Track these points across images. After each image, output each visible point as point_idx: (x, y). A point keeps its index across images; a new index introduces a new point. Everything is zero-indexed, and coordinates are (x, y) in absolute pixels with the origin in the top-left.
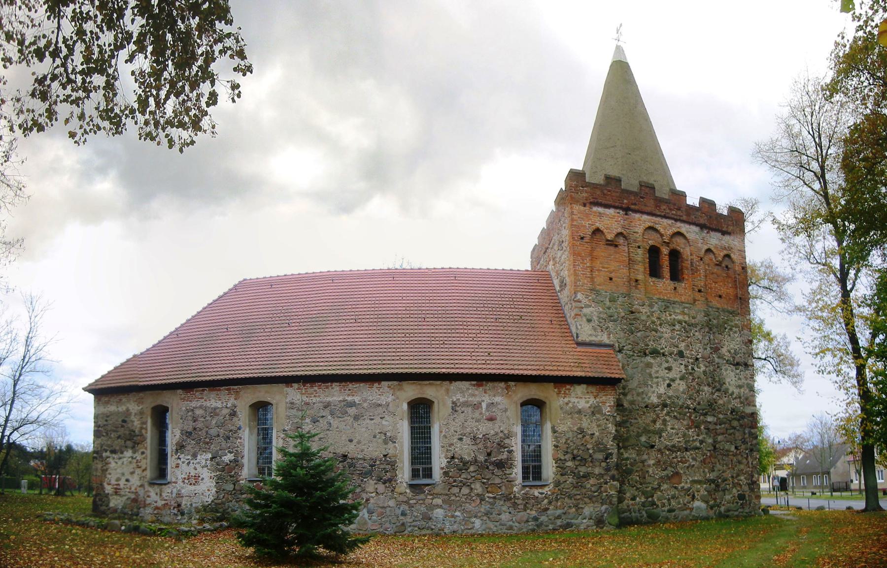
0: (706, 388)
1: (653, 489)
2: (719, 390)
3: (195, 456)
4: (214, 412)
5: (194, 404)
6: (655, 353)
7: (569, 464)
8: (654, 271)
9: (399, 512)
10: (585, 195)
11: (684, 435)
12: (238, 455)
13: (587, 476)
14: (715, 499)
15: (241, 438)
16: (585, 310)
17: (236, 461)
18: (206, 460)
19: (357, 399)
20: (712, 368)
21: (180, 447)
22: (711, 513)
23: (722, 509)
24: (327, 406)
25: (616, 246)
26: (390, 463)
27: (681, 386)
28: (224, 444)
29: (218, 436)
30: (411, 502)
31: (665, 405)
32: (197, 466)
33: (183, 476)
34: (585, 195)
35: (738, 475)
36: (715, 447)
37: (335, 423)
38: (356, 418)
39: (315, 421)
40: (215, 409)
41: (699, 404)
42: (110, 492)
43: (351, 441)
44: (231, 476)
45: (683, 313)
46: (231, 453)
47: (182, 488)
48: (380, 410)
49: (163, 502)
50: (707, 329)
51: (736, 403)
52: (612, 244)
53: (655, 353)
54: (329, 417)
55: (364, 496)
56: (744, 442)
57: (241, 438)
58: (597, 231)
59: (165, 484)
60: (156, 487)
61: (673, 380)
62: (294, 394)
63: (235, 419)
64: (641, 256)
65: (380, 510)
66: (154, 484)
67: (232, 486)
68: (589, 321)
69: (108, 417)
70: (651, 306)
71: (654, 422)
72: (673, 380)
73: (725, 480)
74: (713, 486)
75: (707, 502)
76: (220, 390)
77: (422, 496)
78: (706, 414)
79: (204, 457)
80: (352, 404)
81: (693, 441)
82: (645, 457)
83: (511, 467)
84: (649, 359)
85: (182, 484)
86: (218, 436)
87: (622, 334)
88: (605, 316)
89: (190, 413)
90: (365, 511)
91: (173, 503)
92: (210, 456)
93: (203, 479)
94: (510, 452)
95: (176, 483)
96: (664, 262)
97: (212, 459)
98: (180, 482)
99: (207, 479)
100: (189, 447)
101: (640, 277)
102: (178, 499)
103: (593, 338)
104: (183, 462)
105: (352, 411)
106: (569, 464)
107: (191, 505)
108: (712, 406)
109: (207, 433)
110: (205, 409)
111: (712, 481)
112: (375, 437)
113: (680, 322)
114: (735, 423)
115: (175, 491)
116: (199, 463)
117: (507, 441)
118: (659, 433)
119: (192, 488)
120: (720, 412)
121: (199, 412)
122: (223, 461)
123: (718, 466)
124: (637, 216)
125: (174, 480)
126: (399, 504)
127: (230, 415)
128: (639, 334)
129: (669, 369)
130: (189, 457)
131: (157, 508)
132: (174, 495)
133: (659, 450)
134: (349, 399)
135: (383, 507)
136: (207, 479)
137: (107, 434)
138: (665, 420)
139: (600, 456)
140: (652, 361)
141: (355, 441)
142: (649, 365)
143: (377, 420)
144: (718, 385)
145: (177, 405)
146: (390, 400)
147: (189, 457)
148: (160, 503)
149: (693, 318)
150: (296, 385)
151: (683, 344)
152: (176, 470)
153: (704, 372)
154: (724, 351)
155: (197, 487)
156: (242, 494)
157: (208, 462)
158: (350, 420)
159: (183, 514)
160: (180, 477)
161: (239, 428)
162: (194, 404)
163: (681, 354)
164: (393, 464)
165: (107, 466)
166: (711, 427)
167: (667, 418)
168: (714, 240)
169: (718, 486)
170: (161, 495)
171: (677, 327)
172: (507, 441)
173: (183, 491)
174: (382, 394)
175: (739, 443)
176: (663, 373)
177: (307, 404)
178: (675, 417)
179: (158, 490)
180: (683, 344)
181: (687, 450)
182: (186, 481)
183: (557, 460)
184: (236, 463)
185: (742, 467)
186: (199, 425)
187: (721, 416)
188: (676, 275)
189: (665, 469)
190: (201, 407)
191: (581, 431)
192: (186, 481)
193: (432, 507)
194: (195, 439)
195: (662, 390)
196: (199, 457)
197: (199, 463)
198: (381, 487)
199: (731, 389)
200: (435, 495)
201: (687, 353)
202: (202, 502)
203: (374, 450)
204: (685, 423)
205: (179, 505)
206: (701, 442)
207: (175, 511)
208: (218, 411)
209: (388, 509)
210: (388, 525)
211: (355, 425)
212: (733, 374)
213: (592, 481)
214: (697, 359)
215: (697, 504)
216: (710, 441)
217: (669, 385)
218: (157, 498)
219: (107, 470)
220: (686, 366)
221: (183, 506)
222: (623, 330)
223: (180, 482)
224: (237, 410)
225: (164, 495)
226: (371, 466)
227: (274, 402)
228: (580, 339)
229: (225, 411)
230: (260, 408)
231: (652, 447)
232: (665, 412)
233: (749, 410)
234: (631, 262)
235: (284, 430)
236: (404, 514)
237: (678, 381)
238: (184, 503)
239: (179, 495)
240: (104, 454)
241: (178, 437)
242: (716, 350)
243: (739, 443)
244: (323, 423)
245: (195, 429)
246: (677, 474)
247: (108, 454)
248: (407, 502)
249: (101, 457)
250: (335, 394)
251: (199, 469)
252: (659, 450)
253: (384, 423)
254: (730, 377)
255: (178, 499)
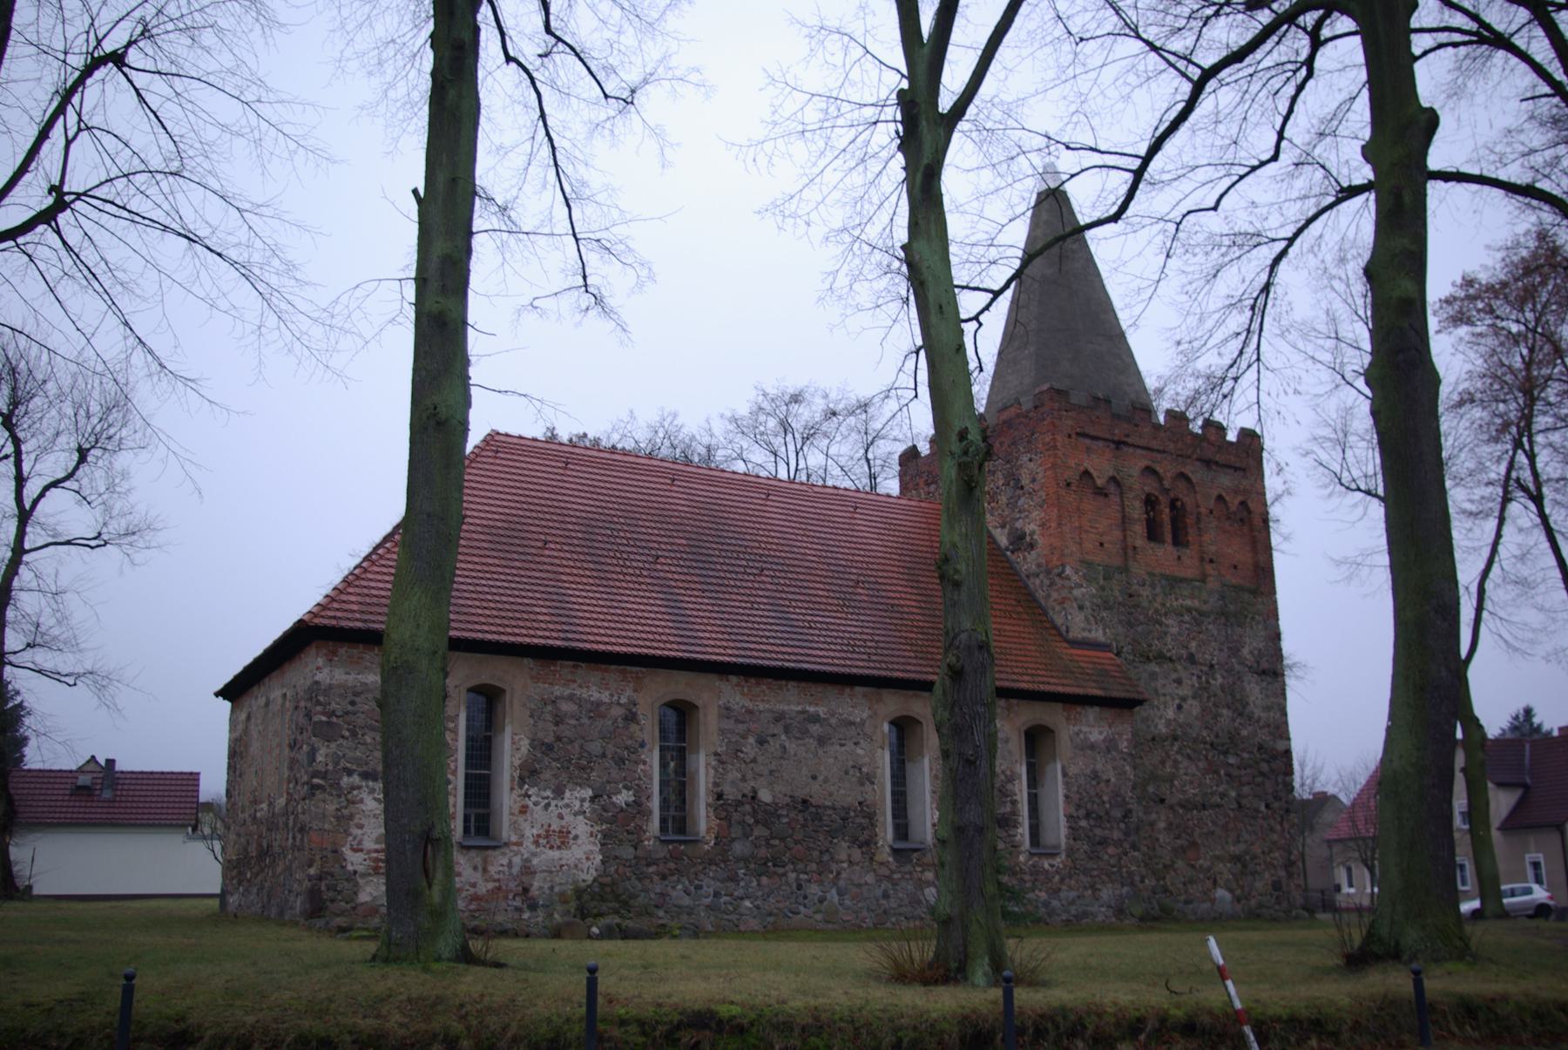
0: (1225, 711)
1: (1165, 866)
2: (1241, 714)
3: (559, 792)
4: (596, 710)
5: (558, 690)
6: (1161, 657)
7: (1083, 823)
8: (1153, 534)
9: (879, 892)
10: (1070, 422)
11: (1200, 785)
12: (641, 793)
13: (1104, 842)
14: (1242, 888)
15: (645, 763)
16: (1077, 592)
17: (637, 803)
18: (583, 800)
19: (821, 711)
20: (1231, 680)
21: (528, 774)
22: (1238, 907)
23: (1253, 902)
24: (779, 717)
25: (1106, 495)
26: (868, 814)
27: (1193, 707)
28: (615, 774)
29: (604, 755)
30: (896, 876)
31: (1175, 739)
32: (564, 811)
33: (535, 832)
34: (1070, 422)
35: (1271, 851)
36: (1239, 803)
37: (792, 747)
38: (822, 741)
39: (761, 742)
40: (599, 704)
41: (1217, 736)
42: (361, 869)
43: (814, 778)
44: (629, 832)
45: (1192, 597)
46: (628, 788)
47: (534, 854)
48: (852, 731)
49: (490, 885)
50: (1223, 620)
51: (1263, 736)
52: (1101, 492)
53: (1161, 657)
54: (783, 737)
55: (834, 867)
56: (1277, 798)
57: (645, 763)
58: (1086, 473)
59: (494, 848)
60: (473, 853)
61: (1184, 699)
62: (732, 694)
63: (634, 727)
64: (1137, 510)
65: (855, 890)
66: (469, 848)
67: (631, 850)
68: (1081, 608)
69: (356, 694)
70: (1153, 586)
71: (1163, 763)
72: (1184, 699)
73: (1254, 857)
74: (1239, 866)
75: (1231, 891)
76: (606, 671)
77: (908, 868)
78: (1226, 753)
79: (578, 796)
80: (815, 719)
81: (1213, 794)
82: (1154, 816)
83: (1016, 825)
84: (1154, 667)
85: (533, 848)
86: (604, 755)
87: (1120, 629)
88: (1099, 601)
89: (549, 708)
90: (834, 891)
91: (512, 885)
92: (590, 792)
93: (576, 837)
94: (1014, 803)
95: (519, 844)
96: (1168, 520)
97: (592, 799)
98: (528, 844)
99: (583, 838)
100: (547, 775)
101: (1139, 542)
102: (525, 879)
103: (1086, 634)
104: (536, 804)
105: (815, 729)
106: (1083, 823)
107: (551, 888)
108: (1233, 737)
109: (581, 747)
110: (580, 702)
111: (1237, 859)
112: (847, 773)
113: (1189, 610)
114: (1265, 767)
115: (517, 860)
116: (567, 806)
117: (1009, 786)
118: (1171, 779)
119: (556, 854)
120: (1243, 750)
121: (566, 707)
122: (614, 804)
123: (1246, 836)
124: (1131, 450)
125: (514, 838)
126: (880, 879)
127: (626, 719)
128: (1139, 629)
129: (1179, 682)
130: (548, 793)
131: (475, 898)
132: (515, 870)
133: (1171, 808)
134: (812, 709)
135: (859, 886)
136: (583, 838)
137: (354, 734)
138: (1175, 761)
139: (1117, 813)
140: (1157, 669)
141: (821, 778)
142: (1153, 676)
143: (850, 746)
144: (1240, 707)
145: (522, 685)
146: (865, 715)
147: (548, 793)
148: (484, 888)
149: (1205, 602)
150: (734, 679)
151: (1194, 644)
152: (521, 819)
153: (1222, 686)
154: (1245, 651)
155: (565, 854)
156: (648, 865)
157: (587, 804)
158: (812, 743)
159: (533, 907)
160: (530, 832)
161: (642, 745)
162: (558, 690)
163: (1191, 659)
164: (871, 817)
165: (352, 809)
166: (1235, 772)
167: (1179, 758)
168: (1226, 481)
169: (1245, 866)
170: (485, 870)
171: (1186, 618)
172: (1009, 786)
173: (535, 861)
174: (853, 707)
175: (1270, 799)
176: (1171, 688)
177: (750, 712)
178: (1189, 757)
179: (479, 861)
180: (1194, 644)
181: (1204, 807)
182: (542, 841)
183: (1069, 817)
184: (638, 808)
185: (1275, 837)
186: (566, 731)
187: (1245, 755)
188: (1179, 540)
189: (1178, 837)
190: (571, 698)
191: (1095, 775)
192: (542, 841)
193: (921, 884)
194: (553, 762)
195: (1170, 714)
196: (568, 794)
197: (567, 806)
198: (857, 854)
199: (1258, 713)
200: (925, 867)
201: (1199, 657)
202: (575, 882)
203: (846, 795)
204: (1201, 765)
205: (526, 890)
206: (1223, 795)
207: (518, 903)
208: (603, 708)
209: (865, 889)
210: (865, 913)
211: (820, 752)
212: (1257, 689)
213: (1111, 850)
214: (1212, 666)
215: (1221, 893)
216: (1233, 794)
217: (1180, 707)
218: (477, 877)
219: (351, 817)
220: (1199, 677)
221: (534, 892)
222: (1120, 621)
223: (528, 844)
224: (640, 710)
225: (492, 869)
226: (843, 819)
227: (699, 703)
228: (1071, 635)
229: (617, 712)
230: (682, 715)
231: (1162, 801)
232: (1175, 748)
233: (1280, 746)
234: (1125, 521)
235: (716, 754)
236: (886, 896)
237: (1190, 701)
238: (536, 884)
239: (528, 870)
240: (345, 780)
241: (524, 750)
242: (1235, 651)
243: (1270, 799)
244: (773, 746)
245: (559, 739)
246: (1194, 844)
247: (356, 779)
248: (889, 878)
249: (337, 785)
250: (791, 701)
251: (569, 818)
252: (1171, 808)
253: (860, 751)
254: (1254, 691)
255: (525, 879)
